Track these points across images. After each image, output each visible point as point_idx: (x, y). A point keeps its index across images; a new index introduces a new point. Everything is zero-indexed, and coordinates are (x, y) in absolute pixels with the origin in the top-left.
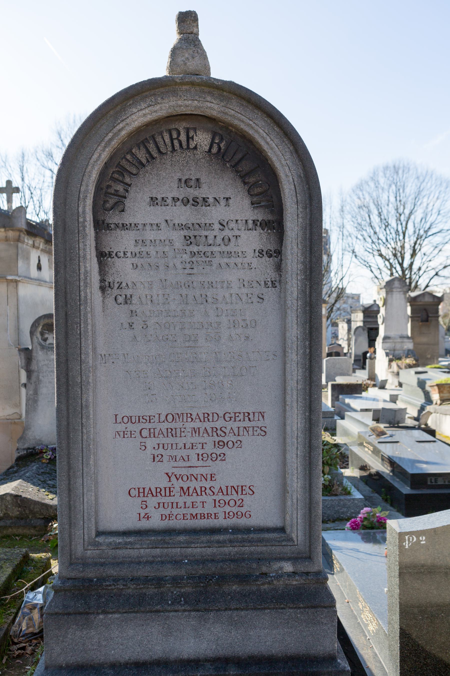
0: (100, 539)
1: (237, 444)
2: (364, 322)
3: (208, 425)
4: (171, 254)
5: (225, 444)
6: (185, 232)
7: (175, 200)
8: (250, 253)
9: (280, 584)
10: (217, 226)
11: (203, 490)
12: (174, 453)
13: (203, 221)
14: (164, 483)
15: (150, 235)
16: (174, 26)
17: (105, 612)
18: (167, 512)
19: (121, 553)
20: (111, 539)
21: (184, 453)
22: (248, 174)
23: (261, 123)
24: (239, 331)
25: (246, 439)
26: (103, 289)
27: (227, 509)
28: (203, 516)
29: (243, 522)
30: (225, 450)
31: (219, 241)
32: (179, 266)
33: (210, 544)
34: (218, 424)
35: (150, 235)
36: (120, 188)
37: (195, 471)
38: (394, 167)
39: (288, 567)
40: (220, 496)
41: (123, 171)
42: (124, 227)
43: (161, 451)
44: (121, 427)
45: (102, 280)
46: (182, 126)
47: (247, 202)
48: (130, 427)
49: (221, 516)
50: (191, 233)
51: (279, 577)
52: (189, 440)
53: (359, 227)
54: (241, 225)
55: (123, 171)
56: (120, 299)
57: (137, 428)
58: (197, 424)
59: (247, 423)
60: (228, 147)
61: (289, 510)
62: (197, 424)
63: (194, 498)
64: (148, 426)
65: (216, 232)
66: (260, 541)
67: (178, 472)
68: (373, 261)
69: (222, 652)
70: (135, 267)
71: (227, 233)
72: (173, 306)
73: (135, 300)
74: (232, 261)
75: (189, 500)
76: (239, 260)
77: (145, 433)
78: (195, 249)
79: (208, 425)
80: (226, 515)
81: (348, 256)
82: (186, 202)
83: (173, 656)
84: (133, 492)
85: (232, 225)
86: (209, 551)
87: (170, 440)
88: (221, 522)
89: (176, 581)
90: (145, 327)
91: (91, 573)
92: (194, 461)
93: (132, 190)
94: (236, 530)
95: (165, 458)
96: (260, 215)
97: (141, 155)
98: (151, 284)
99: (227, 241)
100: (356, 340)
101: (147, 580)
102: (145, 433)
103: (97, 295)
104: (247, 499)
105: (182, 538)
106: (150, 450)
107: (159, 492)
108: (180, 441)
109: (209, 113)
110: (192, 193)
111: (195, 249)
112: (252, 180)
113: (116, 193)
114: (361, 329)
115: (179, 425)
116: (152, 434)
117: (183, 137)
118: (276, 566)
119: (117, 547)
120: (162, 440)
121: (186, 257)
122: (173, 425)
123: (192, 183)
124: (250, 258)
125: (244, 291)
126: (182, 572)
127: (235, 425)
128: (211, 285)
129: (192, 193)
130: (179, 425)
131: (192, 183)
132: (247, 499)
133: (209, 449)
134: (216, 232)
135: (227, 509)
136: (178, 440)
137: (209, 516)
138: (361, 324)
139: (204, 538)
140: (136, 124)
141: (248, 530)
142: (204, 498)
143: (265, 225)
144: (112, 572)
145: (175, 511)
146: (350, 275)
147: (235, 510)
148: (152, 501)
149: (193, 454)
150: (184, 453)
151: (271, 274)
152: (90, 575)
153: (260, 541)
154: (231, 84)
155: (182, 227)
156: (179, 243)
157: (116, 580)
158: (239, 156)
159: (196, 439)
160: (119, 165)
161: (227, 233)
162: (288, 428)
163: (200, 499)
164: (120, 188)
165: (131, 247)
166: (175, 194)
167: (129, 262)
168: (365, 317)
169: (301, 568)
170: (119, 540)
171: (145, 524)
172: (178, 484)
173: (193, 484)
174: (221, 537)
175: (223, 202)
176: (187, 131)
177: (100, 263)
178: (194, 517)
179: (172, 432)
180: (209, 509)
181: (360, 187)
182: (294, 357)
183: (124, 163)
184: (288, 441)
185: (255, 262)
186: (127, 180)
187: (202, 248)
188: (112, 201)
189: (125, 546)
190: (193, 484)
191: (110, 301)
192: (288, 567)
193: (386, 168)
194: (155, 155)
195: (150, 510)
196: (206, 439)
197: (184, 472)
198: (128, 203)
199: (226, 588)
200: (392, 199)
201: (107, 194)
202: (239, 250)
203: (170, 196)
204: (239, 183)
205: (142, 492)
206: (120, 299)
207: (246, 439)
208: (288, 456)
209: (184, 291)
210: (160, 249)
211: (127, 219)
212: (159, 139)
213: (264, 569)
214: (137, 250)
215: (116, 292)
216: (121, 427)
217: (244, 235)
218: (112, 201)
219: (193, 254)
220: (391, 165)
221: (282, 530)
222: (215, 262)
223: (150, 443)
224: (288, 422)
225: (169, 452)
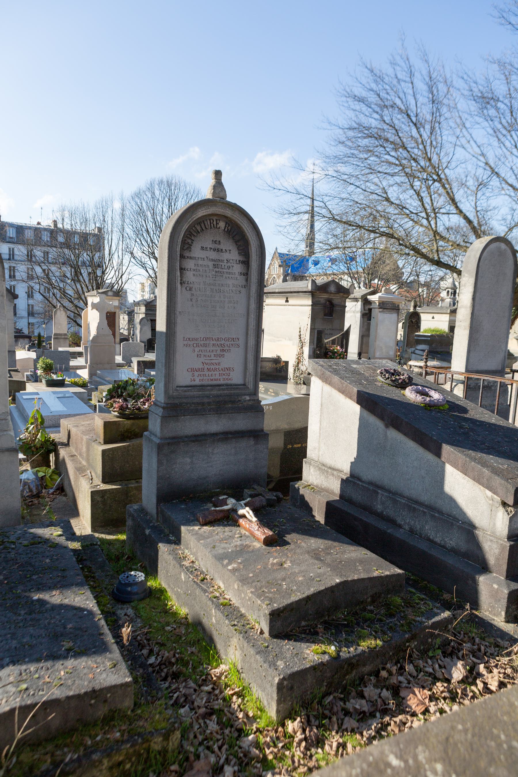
0: (178, 388)
1: (229, 351)
2: (146, 314)
3: (219, 343)
4: (208, 271)
5: (224, 351)
6: (214, 263)
7: (211, 248)
8: (237, 274)
9: (245, 404)
10: (225, 261)
11: (216, 369)
12: (205, 354)
13: (220, 259)
14: (201, 366)
15: (200, 262)
16: (213, 176)
17: (184, 416)
18: (202, 378)
19: (186, 393)
20: (182, 389)
21: (209, 354)
22: (239, 241)
23: (246, 222)
24: (232, 305)
25: (232, 349)
26: (181, 283)
27: (224, 377)
28: (215, 380)
29: (229, 382)
30: (224, 353)
31: (226, 267)
32: (211, 276)
33: (219, 390)
34: (223, 342)
35: (200, 262)
36: (190, 241)
37: (213, 361)
38: (168, 182)
39: (248, 398)
40: (222, 372)
41: (191, 234)
42: (191, 258)
43: (200, 353)
44: (186, 343)
45: (181, 280)
46: (215, 218)
47: (237, 252)
48: (189, 342)
49: (222, 380)
50: (216, 263)
51: (245, 401)
52: (212, 348)
53: (138, 232)
54: (234, 261)
55: (191, 234)
56: (188, 289)
57: (191, 343)
58: (215, 342)
59: (233, 342)
60: (231, 229)
61: (247, 376)
62: (215, 342)
63: (212, 372)
64: (196, 342)
65: (225, 264)
66: (237, 388)
67: (206, 361)
68: (149, 263)
69: (226, 429)
70: (194, 275)
71: (229, 264)
72: (208, 293)
73: (193, 289)
74: (231, 276)
75: (210, 373)
76: (233, 276)
77: (195, 345)
78: (217, 270)
79: (219, 343)
80: (224, 379)
81: (127, 257)
82: (214, 250)
83: (208, 432)
84: (189, 370)
85: (231, 261)
86: (219, 392)
87: (204, 348)
88: (222, 382)
89: (209, 403)
90: (197, 301)
91: (176, 401)
92: (213, 358)
93: (194, 243)
94: (227, 385)
95: (202, 356)
96: (242, 259)
97: (199, 228)
98: (200, 283)
99: (229, 268)
100: (141, 329)
101: (198, 404)
102: (195, 345)
103: (179, 286)
104: (231, 373)
105: (209, 388)
106: (196, 353)
107: (198, 370)
108: (208, 349)
109: (227, 215)
110: (217, 246)
111: (217, 270)
112: (239, 244)
113: (188, 243)
114: (145, 320)
115: (207, 342)
116: (197, 346)
117: (215, 223)
118: (243, 397)
119: (185, 391)
120: (201, 348)
121: (214, 273)
122: (205, 342)
123: (217, 242)
124: (237, 275)
125: (234, 288)
126: (211, 400)
127: (228, 343)
128: (222, 285)
129: (217, 246)
130: (207, 342)
131: (217, 242)
132: (231, 373)
133: (219, 352)
134: (225, 264)
135: (224, 377)
136: (207, 348)
137: (217, 379)
138: (144, 316)
139: (217, 388)
140: (200, 216)
141: (231, 385)
142: (216, 372)
143: (243, 262)
144: (185, 401)
145: (205, 378)
146: (129, 274)
147: (227, 377)
148: (196, 374)
149: (212, 354)
150: (209, 354)
151: (244, 283)
152: (177, 402)
153: (237, 388)
154: (235, 204)
155: (213, 260)
156: (211, 267)
157: (187, 404)
158: (235, 233)
159: (214, 348)
160: (190, 232)
161: (229, 264)
162: (249, 344)
163: (214, 373)
164: (190, 241)
165: (193, 267)
166: (211, 246)
167: (192, 273)
168: (146, 310)
169: (252, 398)
170: (185, 389)
171: (193, 383)
172: (206, 367)
173: (212, 367)
174: (223, 387)
175: (228, 251)
176: (217, 220)
177: (180, 272)
178: (212, 380)
179: (205, 345)
180: (217, 377)
181: (138, 195)
182: (252, 316)
183: (192, 231)
184: (249, 349)
185: (239, 277)
186: (193, 238)
187: (220, 270)
188: (186, 246)
189: (188, 391)
190: (212, 367)
191: (184, 289)
192: (248, 398)
193: (161, 182)
194: (204, 229)
195: (195, 377)
196: (218, 348)
197: (209, 361)
198: (192, 247)
199: (227, 406)
200: (166, 210)
201: (184, 243)
202: (233, 272)
203: (209, 247)
204: (234, 244)
205: (193, 370)
206: (188, 289)
207: (232, 349)
208: (248, 355)
209: (212, 287)
210: (204, 268)
211: (192, 255)
212: (206, 222)
213: (240, 399)
214: (195, 268)
215: (186, 285)
216: (186, 343)
217: (235, 265)
218: (186, 246)
219: (216, 272)
220: (165, 180)
221: (244, 385)
222: (224, 276)
223: (197, 349)
224: (249, 342)
225: (204, 353)
